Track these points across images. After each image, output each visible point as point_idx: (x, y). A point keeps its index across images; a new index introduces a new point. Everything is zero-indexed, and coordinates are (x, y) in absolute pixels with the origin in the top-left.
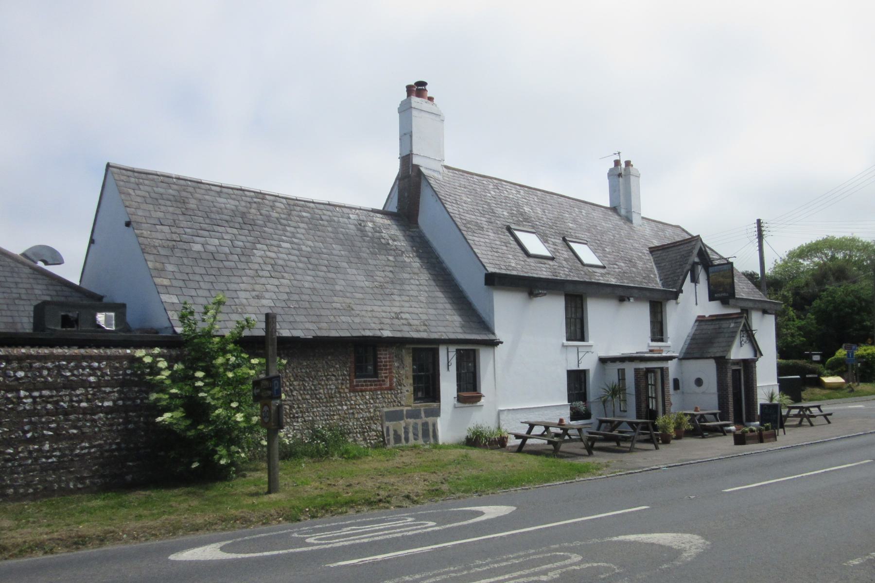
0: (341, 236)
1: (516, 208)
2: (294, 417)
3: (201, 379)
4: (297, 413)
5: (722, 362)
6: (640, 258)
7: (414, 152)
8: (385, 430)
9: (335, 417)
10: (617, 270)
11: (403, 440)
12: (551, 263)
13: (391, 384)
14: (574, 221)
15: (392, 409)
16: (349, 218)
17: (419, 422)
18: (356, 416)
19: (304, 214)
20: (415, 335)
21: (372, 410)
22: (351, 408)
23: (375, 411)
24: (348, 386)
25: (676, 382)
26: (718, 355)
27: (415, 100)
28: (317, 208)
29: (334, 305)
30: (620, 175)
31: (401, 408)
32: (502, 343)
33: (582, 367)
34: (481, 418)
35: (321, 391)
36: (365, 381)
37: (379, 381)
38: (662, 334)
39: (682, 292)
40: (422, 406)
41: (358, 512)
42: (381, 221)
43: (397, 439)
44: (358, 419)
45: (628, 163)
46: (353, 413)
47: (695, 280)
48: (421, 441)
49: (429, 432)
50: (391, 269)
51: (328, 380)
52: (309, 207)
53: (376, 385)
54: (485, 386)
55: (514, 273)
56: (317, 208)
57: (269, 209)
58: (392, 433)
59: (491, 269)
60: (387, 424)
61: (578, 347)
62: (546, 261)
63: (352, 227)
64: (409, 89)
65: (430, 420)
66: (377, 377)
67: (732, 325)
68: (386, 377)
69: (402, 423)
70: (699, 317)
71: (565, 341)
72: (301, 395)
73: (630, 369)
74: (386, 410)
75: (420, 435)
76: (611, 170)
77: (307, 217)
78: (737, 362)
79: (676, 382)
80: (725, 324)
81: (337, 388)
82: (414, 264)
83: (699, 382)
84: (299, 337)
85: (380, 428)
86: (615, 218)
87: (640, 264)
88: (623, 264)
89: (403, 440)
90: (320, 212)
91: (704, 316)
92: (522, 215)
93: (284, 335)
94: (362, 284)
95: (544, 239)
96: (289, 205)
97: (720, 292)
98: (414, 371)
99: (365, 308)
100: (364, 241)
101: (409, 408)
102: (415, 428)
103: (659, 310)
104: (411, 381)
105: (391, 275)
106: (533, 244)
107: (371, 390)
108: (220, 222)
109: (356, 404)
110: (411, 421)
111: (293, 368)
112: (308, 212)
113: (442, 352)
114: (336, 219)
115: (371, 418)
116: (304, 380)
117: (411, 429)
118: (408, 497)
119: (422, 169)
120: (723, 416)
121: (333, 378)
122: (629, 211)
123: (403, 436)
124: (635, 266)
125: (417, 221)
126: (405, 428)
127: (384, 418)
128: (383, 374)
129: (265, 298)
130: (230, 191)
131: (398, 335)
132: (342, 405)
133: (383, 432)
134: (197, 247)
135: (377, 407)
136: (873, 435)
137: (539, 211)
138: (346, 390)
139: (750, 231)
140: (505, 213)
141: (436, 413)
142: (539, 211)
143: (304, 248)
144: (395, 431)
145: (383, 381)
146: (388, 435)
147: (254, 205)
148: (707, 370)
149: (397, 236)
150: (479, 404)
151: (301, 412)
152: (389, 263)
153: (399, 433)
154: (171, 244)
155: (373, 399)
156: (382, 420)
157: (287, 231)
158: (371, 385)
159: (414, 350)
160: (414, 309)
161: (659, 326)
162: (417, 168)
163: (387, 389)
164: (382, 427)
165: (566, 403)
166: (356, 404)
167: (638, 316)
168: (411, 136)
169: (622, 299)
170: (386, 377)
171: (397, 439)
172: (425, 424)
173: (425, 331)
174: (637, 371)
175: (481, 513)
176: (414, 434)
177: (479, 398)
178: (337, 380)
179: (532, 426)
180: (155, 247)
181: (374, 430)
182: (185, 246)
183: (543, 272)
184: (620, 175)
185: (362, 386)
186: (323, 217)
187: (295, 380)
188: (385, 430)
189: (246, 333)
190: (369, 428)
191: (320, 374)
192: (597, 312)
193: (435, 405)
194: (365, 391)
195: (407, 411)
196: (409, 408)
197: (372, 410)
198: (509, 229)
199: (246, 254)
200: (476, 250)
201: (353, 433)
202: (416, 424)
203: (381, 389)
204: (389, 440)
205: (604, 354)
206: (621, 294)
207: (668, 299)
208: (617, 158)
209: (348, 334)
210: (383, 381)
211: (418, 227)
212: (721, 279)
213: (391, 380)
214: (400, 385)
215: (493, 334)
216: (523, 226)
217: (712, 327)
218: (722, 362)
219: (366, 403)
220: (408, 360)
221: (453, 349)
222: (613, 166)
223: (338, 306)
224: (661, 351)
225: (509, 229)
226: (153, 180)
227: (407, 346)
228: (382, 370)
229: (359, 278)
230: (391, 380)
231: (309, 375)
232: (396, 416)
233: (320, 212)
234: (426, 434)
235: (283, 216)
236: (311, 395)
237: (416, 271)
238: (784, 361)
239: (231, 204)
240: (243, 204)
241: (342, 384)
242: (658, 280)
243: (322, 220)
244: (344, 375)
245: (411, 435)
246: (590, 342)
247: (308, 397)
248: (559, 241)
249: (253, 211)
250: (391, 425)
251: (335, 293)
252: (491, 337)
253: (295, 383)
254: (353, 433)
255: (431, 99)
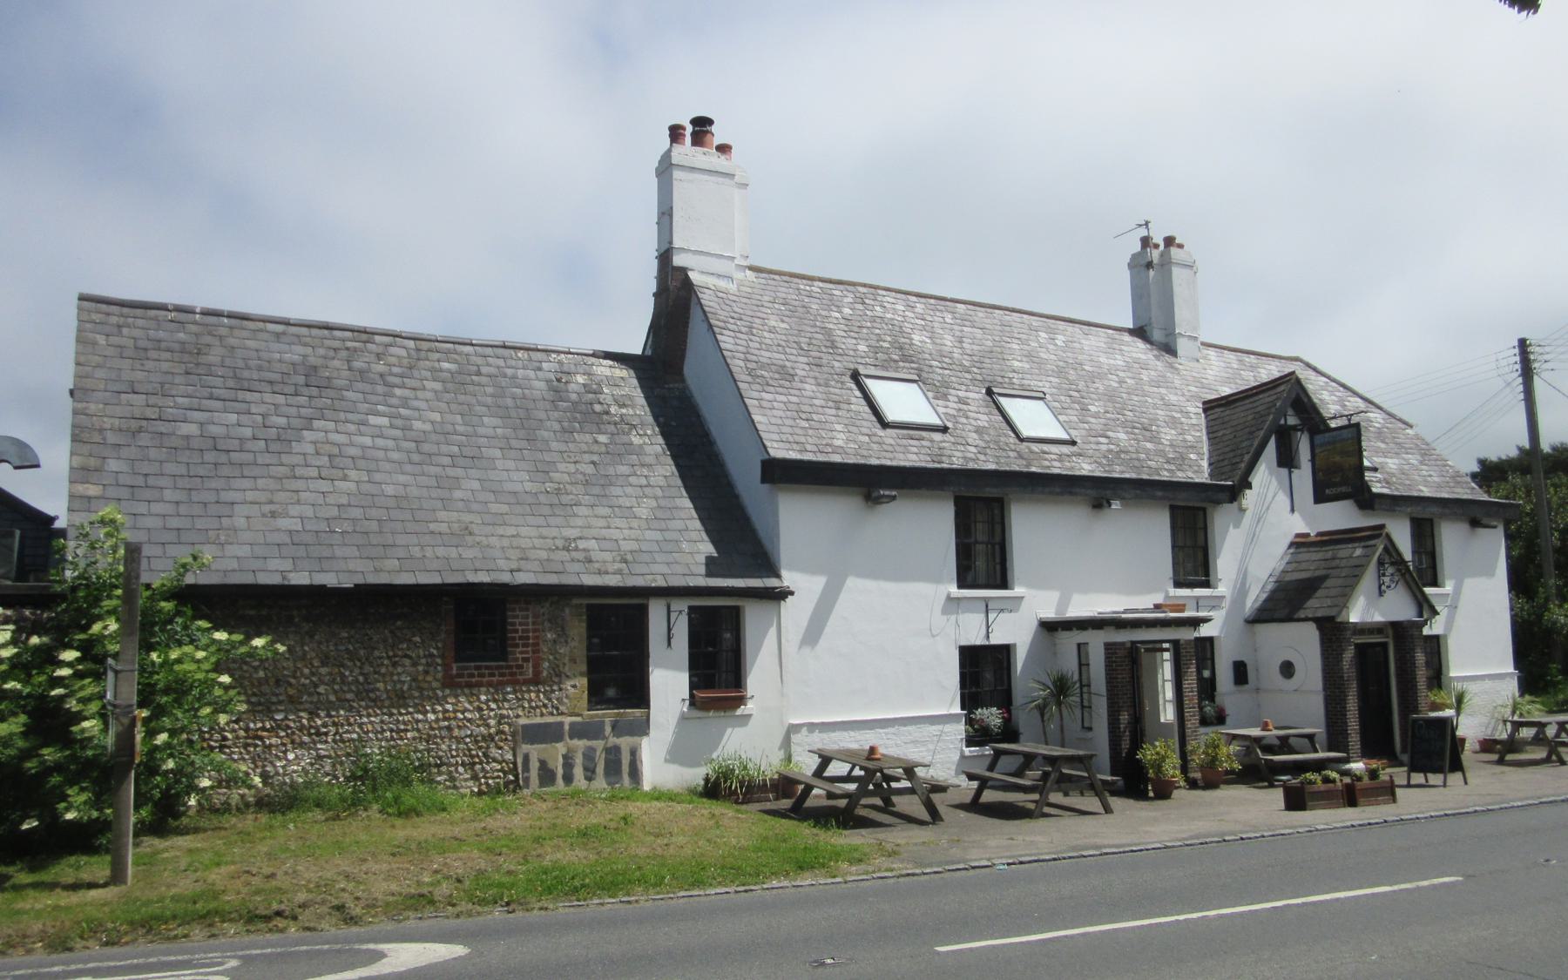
0: (509, 402)
1: (856, 332)
2: (318, 734)
3: (69, 665)
4: (325, 725)
5: (1332, 631)
6: (1173, 423)
7: (677, 243)
8: (520, 761)
9: (409, 735)
10: (1104, 448)
11: (560, 781)
12: (937, 436)
13: (537, 673)
14: (1030, 356)
15: (538, 720)
16: (540, 369)
17: (599, 744)
18: (456, 732)
19: (446, 365)
20: (589, 580)
21: (492, 722)
22: (445, 719)
23: (499, 723)
24: (440, 675)
25: (1241, 673)
26: (1319, 614)
27: (685, 152)
28: (476, 354)
29: (432, 526)
30: (1149, 265)
31: (559, 719)
32: (792, 593)
33: (996, 639)
34: (753, 740)
35: (380, 685)
36: (477, 668)
37: (510, 667)
38: (1207, 574)
39: (1249, 486)
40: (607, 715)
41: (213, 936)
42: (607, 372)
43: (547, 776)
44: (459, 740)
45: (1169, 241)
46: (449, 728)
47: (1287, 460)
48: (600, 782)
49: (624, 768)
50: (595, 458)
51: (395, 665)
52: (459, 354)
53: (502, 675)
54: (759, 676)
55: (837, 458)
56: (476, 354)
57: (373, 358)
58: (534, 765)
59: (778, 451)
60: (525, 748)
61: (986, 601)
62: (924, 434)
63: (542, 385)
64: (675, 133)
65: (625, 742)
66: (505, 660)
67: (1358, 552)
68: (526, 660)
69: (561, 748)
70: (1298, 535)
71: (953, 589)
72: (335, 692)
73: (1096, 642)
74: (523, 721)
75: (600, 769)
76: (1134, 257)
77: (449, 371)
78: (1361, 629)
79: (1241, 673)
80: (1344, 551)
81: (414, 680)
82: (648, 449)
83: (1287, 669)
84: (323, 587)
85: (509, 756)
86: (1138, 348)
87: (1168, 435)
88: (1122, 436)
89: (560, 781)
90: (479, 361)
91: (1308, 535)
92: (901, 348)
93: (293, 582)
94: (518, 487)
95: (937, 391)
96: (418, 350)
97: (1335, 485)
98: (590, 648)
99: (500, 530)
100: (556, 408)
101: (579, 719)
102: (589, 756)
103: (1200, 524)
104: (584, 668)
105: (590, 469)
106: (902, 401)
107: (490, 684)
108: (256, 386)
109: (455, 711)
110: (580, 744)
111: (320, 643)
112: (455, 362)
113: (656, 613)
114: (509, 372)
115: (491, 737)
116: (343, 665)
117: (579, 760)
118: (340, 908)
119: (692, 275)
120: (1336, 738)
121: (407, 662)
122: (1170, 333)
123: (560, 772)
124: (1154, 439)
125: (682, 369)
126: (565, 757)
127: (519, 738)
128: (518, 654)
129: (287, 516)
130: (304, 331)
131: (552, 580)
132: (425, 713)
133: (515, 764)
134: (191, 429)
135: (502, 716)
136: (1565, 805)
137: (948, 341)
138: (435, 684)
139: (1504, 363)
140: (862, 348)
141: (642, 728)
142: (948, 341)
143: (417, 425)
144: (543, 763)
145: (521, 667)
146: (526, 767)
147: (344, 354)
148: (1300, 642)
149: (630, 397)
150: (739, 712)
151: (335, 724)
152: (595, 448)
153: (551, 765)
154: (134, 424)
155: (495, 701)
156: (515, 741)
157: (393, 396)
158: (492, 675)
159: (589, 607)
160: (644, 531)
161: (1200, 556)
162: (683, 271)
163: (527, 682)
164: (515, 755)
165: (957, 709)
166: (455, 711)
167: (1150, 534)
168: (671, 216)
169: (1099, 504)
170: (526, 660)
171: (547, 776)
172: (613, 754)
173: (619, 572)
174: (1109, 647)
175: (381, 955)
176: (586, 769)
177: (741, 701)
178: (415, 664)
179: (826, 760)
180: (101, 430)
181: (495, 760)
182: (162, 427)
183: (912, 456)
184: (1149, 265)
185: (472, 676)
186: (484, 370)
187: (324, 664)
188: (520, 761)
189: (190, 579)
190: (485, 755)
191: (377, 653)
192: (1032, 531)
193: (637, 712)
194: (479, 685)
195: (572, 725)
196: (579, 719)
197: (492, 722)
198: (855, 376)
199: (283, 440)
200: (756, 418)
201: (449, 765)
202: (592, 749)
203: (514, 683)
204: (527, 780)
205: (1050, 614)
206: (1099, 493)
207: (1218, 502)
208: (1143, 232)
209: (438, 580)
210: (521, 667)
211: (683, 381)
212: (1338, 459)
213: (536, 667)
214: (559, 675)
215: (778, 576)
216: (896, 370)
217: (1320, 556)
218: (1332, 631)
219: (480, 709)
220: (578, 630)
221: (682, 605)
222: (1137, 247)
223: (443, 528)
224: (1181, 608)
225: (855, 376)
226: (156, 319)
227: (575, 601)
228: (517, 646)
229: (515, 476)
230: (536, 667)
231: (353, 656)
232: (548, 734)
233: (479, 361)
234: (613, 769)
235: (396, 370)
236: (358, 694)
237: (649, 460)
238: (567, 727)
239: (295, 353)
240: (322, 351)
241: (426, 672)
242: (1205, 464)
243: (249, 368)
244: (432, 655)
245: (578, 772)
246: (1018, 590)
247: (350, 696)
248: (977, 395)
249: (336, 363)
250: (535, 751)
251: (446, 503)
252: (772, 582)
253: (323, 670)
254: (449, 765)
255: (723, 149)
